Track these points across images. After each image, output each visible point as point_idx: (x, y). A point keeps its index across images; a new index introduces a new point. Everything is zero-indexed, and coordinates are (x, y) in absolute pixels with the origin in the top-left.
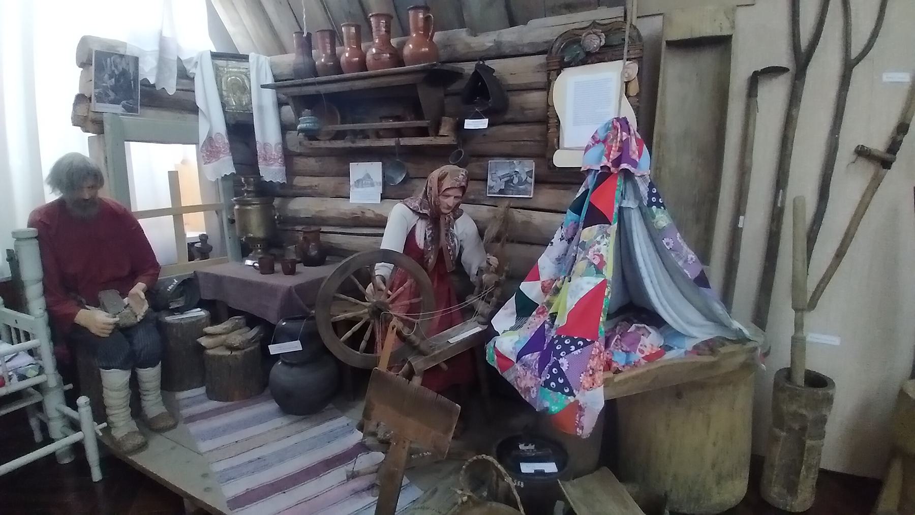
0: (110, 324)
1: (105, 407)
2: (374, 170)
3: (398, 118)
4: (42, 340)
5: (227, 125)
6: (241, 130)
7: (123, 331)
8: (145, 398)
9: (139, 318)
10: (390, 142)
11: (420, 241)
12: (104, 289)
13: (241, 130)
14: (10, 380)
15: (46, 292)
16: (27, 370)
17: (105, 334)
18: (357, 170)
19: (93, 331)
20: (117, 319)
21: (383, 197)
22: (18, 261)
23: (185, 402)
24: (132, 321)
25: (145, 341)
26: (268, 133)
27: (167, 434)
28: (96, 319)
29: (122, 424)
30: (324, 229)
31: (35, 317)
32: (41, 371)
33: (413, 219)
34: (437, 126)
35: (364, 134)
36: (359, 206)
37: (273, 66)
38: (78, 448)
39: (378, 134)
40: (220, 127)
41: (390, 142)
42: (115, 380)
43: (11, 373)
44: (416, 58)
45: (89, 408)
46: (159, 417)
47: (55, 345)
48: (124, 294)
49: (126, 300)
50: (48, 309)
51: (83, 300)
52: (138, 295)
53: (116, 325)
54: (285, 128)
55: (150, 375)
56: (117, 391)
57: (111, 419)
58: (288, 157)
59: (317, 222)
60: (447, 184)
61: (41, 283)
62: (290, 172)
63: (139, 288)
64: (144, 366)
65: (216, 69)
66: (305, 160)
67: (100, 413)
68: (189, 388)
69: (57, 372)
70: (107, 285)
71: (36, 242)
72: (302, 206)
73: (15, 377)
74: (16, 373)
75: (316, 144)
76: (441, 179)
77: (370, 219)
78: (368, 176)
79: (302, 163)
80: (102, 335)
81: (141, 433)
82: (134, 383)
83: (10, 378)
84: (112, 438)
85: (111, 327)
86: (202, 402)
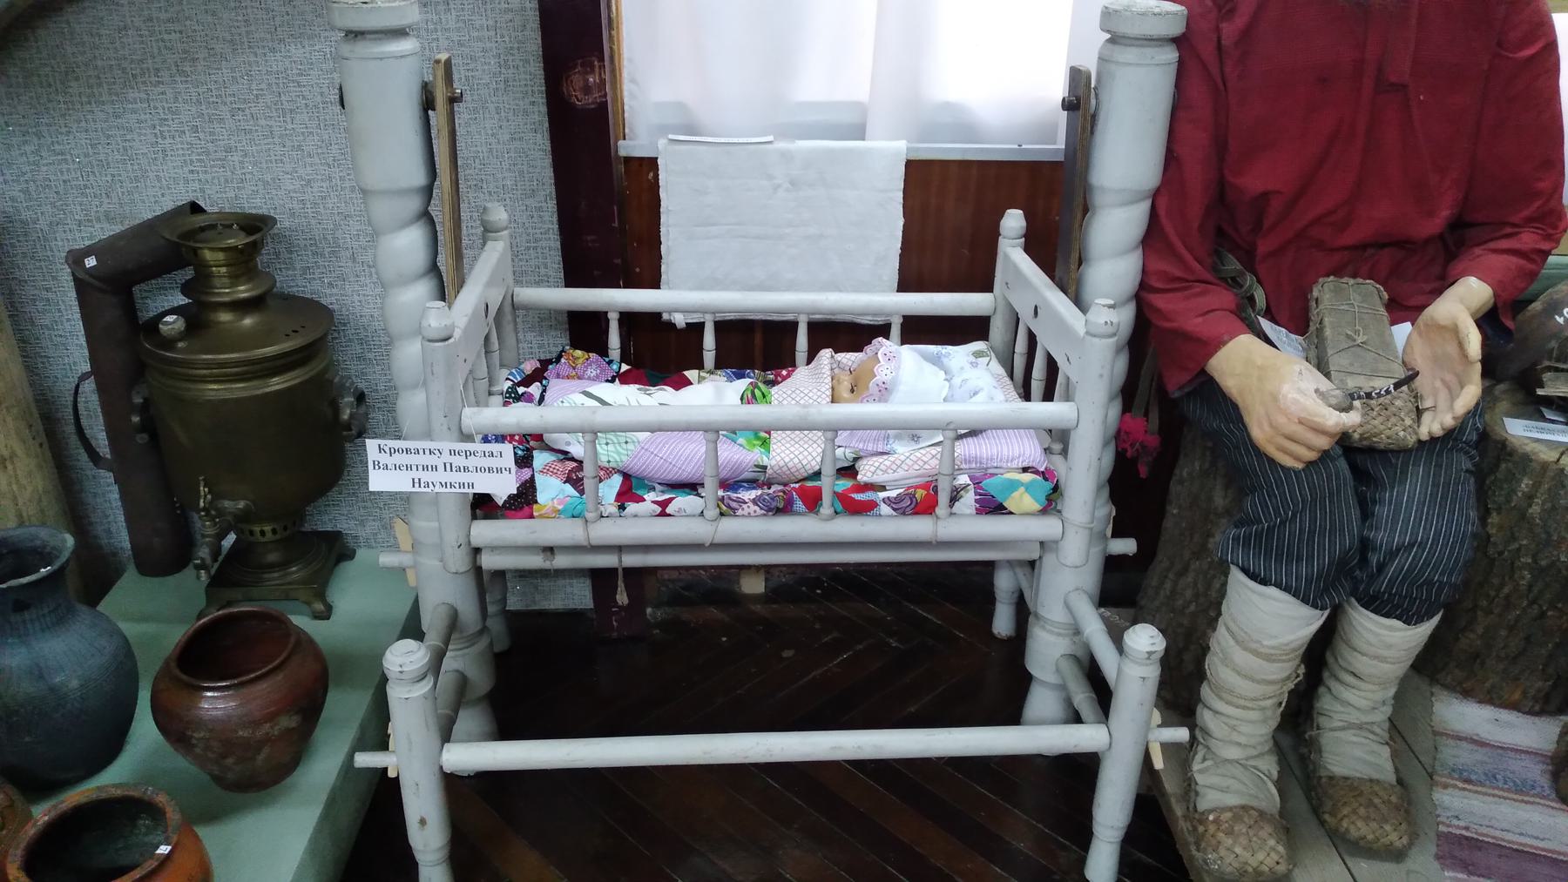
0: (1319, 430)
1: (1200, 675)
4: (1089, 409)
7: (1360, 461)
8: (1333, 684)
9: (1432, 425)
12: (1338, 272)
14: (954, 499)
15: (1153, 239)
16: (1013, 486)
17: (1292, 456)
19: (1259, 432)
20: (1352, 419)
22: (1094, 117)
23: (1464, 756)
24: (1397, 429)
25: (1411, 518)
27: (1363, 867)
28: (1284, 390)
29: (1234, 768)
31: (1088, 329)
32: (1052, 501)
38: (1079, 772)
42: (1263, 623)
43: (963, 479)
45: (1153, 672)
46: (1354, 788)
47: (1127, 408)
48: (1403, 308)
49: (1403, 331)
50: (1142, 296)
51: (1260, 296)
52: (1455, 331)
53: (1344, 442)
55: (1384, 643)
56: (1256, 653)
57: (1205, 717)
61: (1145, 206)
63: (1464, 300)
64: (1380, 605)
67: (1181, 689)
68: (1491, 698)
69: (1106, 492)
70: (1352, 262)
71: (1171, 55)
73: (969, 500)
74: (977, 483)
80: (1288, 462)
81: (1286, 826)
82: (1319, 656)
83: (954, 498)
84: (1189, 788)
85: (1324, 443)
86: (1521, 790)
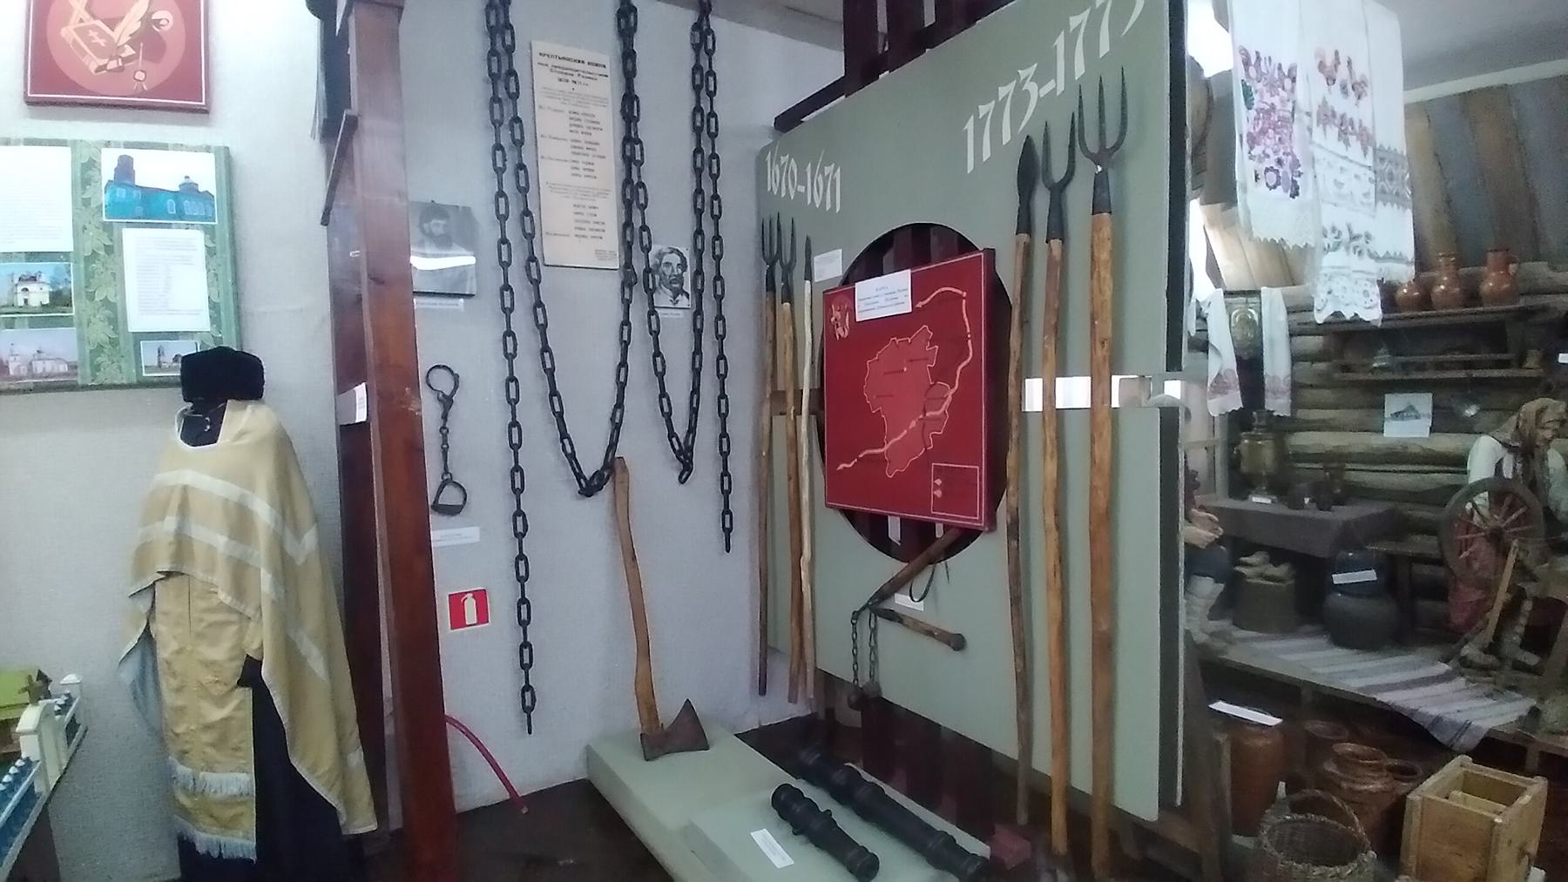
2: (1424, 402)
3: (1463, 350)
5: (1239, 360)
6: (1250, 365)
10: (1462, 374)
11: (1508, 473)
13: (1250, 365)
18: (1393, 402)
21: (1432, 430)
26: (1277, 366)
30: (1349, 466)
33: (1501, 452)
34: (1521, 363)
35: (1421, 367)
36: (1399, 440)
37: (1285, 297)
39: (1440, 366)
40: (1232, 364)
41: (1462, 374)
44: (1497, 298)
54: (1295, 359)
58: (1296, 387)
59: (1335, 460)
60: (1547, 417)
62: (1295, 405)
65: (1228, 307)
66: (1314, 391)
72: (1304, 440)
75: (1351, 376)
76: (1541, 411)
77: (1416, 455)
78: (1412, 408)
79: (1309, 395)
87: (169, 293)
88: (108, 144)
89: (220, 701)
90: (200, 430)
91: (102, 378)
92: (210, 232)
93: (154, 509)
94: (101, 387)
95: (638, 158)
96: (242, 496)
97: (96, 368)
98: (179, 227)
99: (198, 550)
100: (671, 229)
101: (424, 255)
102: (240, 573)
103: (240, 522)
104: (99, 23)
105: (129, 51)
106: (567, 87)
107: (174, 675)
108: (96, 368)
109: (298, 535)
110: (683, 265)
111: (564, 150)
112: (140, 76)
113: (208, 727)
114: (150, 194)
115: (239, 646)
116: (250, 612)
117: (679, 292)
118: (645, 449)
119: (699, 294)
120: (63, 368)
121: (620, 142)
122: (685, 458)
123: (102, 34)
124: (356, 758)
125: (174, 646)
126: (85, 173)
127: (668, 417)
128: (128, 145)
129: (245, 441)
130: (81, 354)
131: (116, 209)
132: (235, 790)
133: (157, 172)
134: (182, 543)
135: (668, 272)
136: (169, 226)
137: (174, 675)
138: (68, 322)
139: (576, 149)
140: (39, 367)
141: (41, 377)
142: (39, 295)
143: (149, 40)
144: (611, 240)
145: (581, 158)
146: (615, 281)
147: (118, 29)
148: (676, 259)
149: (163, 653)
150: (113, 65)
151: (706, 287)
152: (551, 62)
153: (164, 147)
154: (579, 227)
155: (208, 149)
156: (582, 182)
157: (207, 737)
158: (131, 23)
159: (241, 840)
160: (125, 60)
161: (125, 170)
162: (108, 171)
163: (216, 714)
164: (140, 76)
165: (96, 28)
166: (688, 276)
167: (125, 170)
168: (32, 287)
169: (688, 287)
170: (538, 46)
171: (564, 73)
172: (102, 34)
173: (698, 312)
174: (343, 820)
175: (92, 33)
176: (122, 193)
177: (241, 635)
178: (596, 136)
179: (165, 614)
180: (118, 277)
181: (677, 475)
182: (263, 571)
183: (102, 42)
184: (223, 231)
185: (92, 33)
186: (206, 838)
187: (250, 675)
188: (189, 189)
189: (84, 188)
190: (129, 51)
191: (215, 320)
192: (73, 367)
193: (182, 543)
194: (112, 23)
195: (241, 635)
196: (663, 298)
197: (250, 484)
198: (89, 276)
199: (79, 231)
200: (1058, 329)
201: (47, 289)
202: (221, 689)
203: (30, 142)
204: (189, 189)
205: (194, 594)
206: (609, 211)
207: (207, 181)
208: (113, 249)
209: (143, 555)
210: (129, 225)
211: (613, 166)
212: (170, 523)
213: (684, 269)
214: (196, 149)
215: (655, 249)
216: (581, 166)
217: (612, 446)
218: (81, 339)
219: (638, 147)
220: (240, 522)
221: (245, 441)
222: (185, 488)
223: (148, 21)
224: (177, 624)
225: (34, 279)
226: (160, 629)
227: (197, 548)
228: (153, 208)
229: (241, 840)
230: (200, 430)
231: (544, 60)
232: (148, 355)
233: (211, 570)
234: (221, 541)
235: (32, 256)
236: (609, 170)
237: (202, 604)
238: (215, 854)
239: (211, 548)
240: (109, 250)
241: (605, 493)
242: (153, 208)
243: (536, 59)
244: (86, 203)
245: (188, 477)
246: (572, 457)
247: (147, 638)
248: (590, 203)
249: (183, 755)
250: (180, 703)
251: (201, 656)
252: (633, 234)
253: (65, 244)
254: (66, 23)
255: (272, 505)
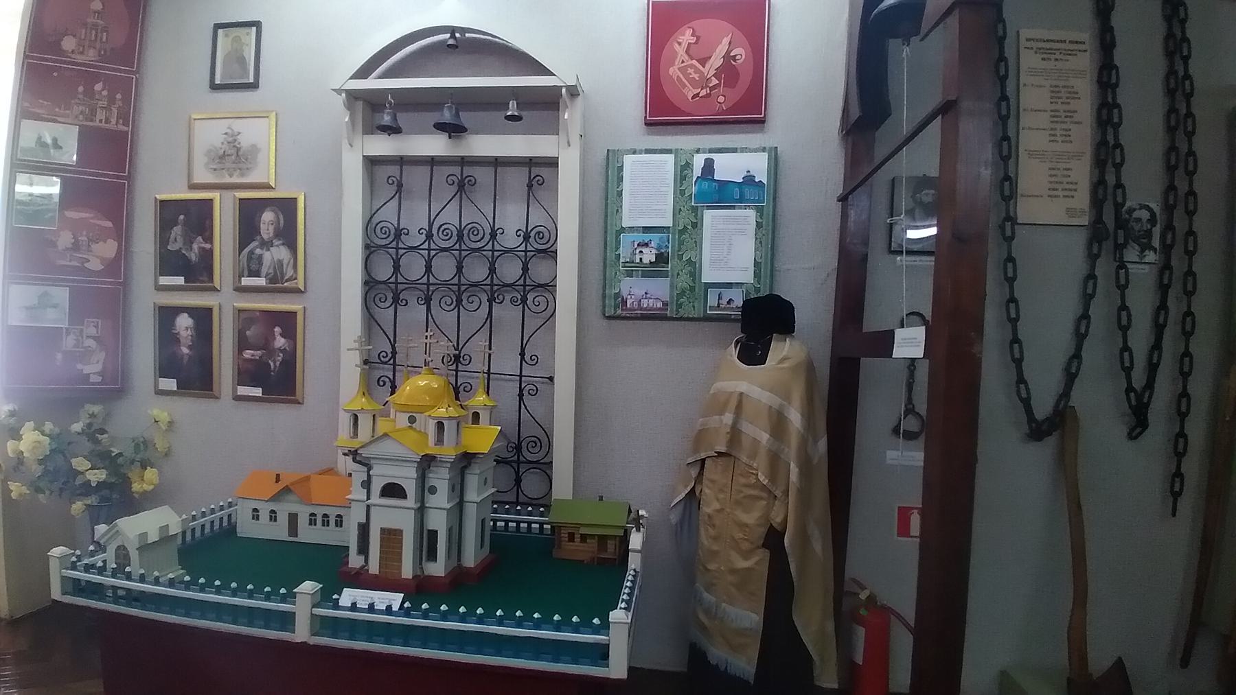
87: (729, 253)
88: (698, 151)
89: (746, 555)
90: (753, 353)
91: (682, 313)
92: (760, 210)
93: (717, 405)
94: (681, 319)
95: (1116, 120)
96: (781, 405)
97: (679, 306)
98: (740, 208)
99: (746, 443)
100: (1143, 188)
101: (917, 228)
102: (775, 460)
103: (778, 424)
104: (694, 62)
105: (715, 81)
106: (1050, 65)
107: (714, 526)
108: (679, 306)
109: (816, 442)
110: (1153, 220)
111: (1043, 120)
112: (721, 99)
113: (733, 571)
114: (723, 184)
115: (766, 516)
116: (778, 493)
117: (1146, 247)
118: (1098, 401)
119: (1167, 249)
120: (659, 305)
121: (1096, 107)
122: (1139, 421)
123: (697, 71)
124: (830, 626)
125: (717, 506)
126: (683, 170)
127: (1128, 371)
128: (711, 151)
129: (786, 365)
130: (671, 297)
131: (701, 196)
132: (747, 625)
133: (730, 167)
134: (735, 434)
135: (1137, 227)
136: (733, 207)
137: (714, 526)
138: (664, 274)
139: (1055, 115)
140: (645, 303)
141: (645, 309)
142: (649, 256)
143: (728, 71)
144: (1082, 199)
145: (1058, 126)
146: (1079, 241)
147: (708, 66)
148: (1145, 215)
149: (707, 509)
150: (703, 93)
151: (1176, 242)
152: (1035, 45)
153: (734, 150)
154: (1052, 192)
155: (764, 150)
156: (1059, 147)
157: (730, 578)
158: (716, 61)
159: (744, 664)
160: (712, 88)
161: (709, 166)
162: (697, 170)
163: (742, 564)
164: (721, 99)
165: (692, 66)
166: (1157, 231)
167: (709, 166)
168: (645, 250)
169: (1156, 243)
170: (1025, 33)
171: (1046, 54)
172: (697, 71)
173: (1166, 267)
174: (816, 672)
175: (690, 71)
176: (706, 185)
177: (769, 508)
178: (1074, 105)
179: (712, 481)
180: (698, 244)
181: (1126, 431)
182: (792, 465)
183: (696, 76)
184: (768, 211)
185: (690, 71)
186: (718, 653)
187: (773, 539)
188: (749, 180)
189: (682, 184)
190: (715, 81)
191: (757, 275)
192: (665, 304)
193: (735, 434)
194: (703, 62)
195: (769, 508)
196: (1131, 254)
197: (787, 397)
198: (681, 243)
199: (677, 212)
200: (269, 618)
201: (654, 251)
202: (746, 546)
203: (648, 151)
204: (749, 180)
205: (737, 472)
206: (1082, 172)
207: (761, 176)
208: (697, 225)
209: (700, 438)
210: (709, 208)
211: (1089, 131)
212: (728, 418)
213: (1154, 225)
214: (755, 151)
215: (1128, 204)
216: (1058, 133)
217: (1065, 394)
218: (672, 286)
219: (1116, 111)
220: (778, 424)
221: (786, 365)
222: (742, 394)
223: (728, 58)
224: (721, 491)
225: (646, 245)
226: (707, 492)
227: (744, 438)
228: (724, 195)
229: (744, 664)
230: (753, 353)
231: (1029, 44)
232: (712, 300)
233: (753, 456)
234: (764, 437)
235: (647, 229)
236: (1083, 134)
237: (743, 480)
238: (723, 669)
239: (756, 442)
240: (694, 225)
241: (1051, 442)
242: (724, 195)
243: (1023, 43)
244: (683, 192)
245: (743, 387)
246: (1027, 403)
247: (693, 497)
248: (1065, 166)
249: (709, 587)
250: (715, 548)
251: (733, 517)
252: (1106, 191)
253: (668, 222)
254: (673, 64)
255: (802, 415)
